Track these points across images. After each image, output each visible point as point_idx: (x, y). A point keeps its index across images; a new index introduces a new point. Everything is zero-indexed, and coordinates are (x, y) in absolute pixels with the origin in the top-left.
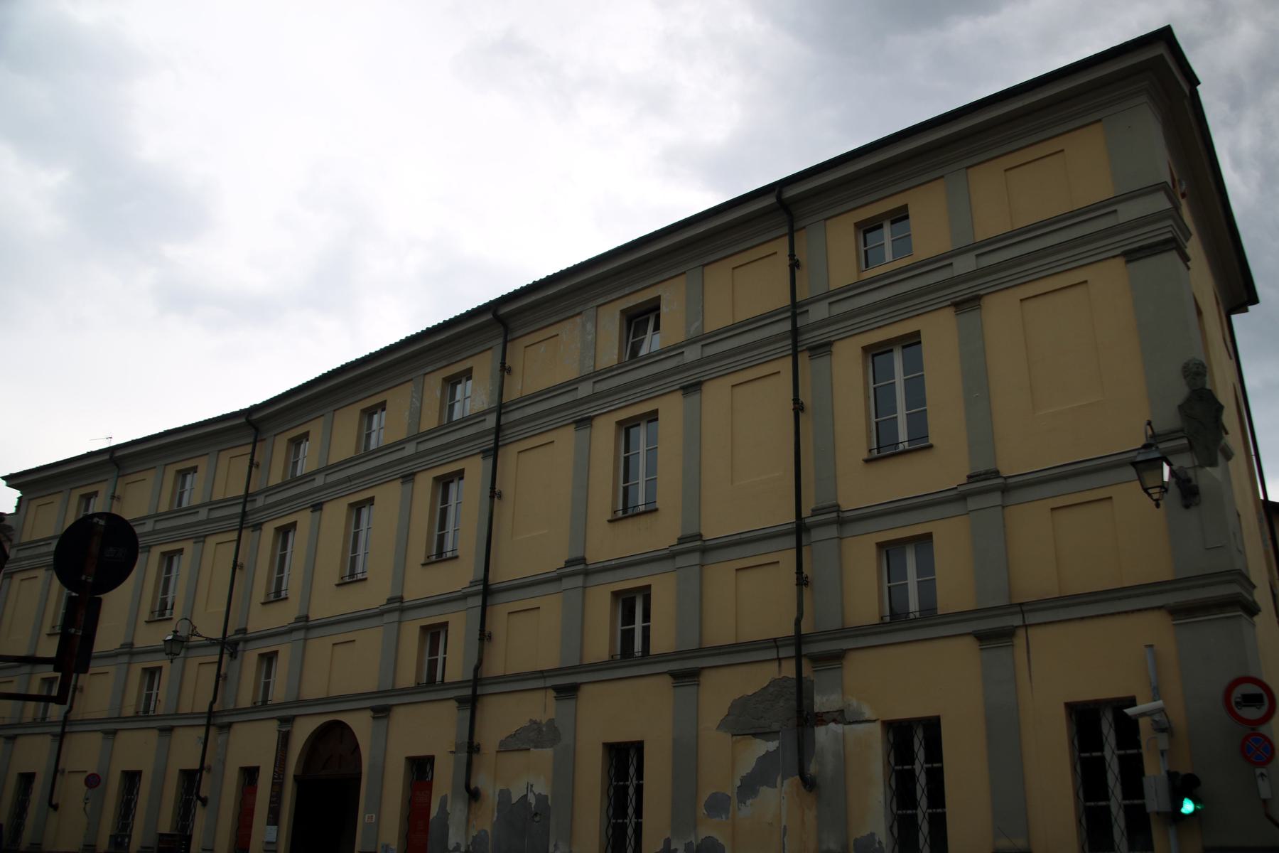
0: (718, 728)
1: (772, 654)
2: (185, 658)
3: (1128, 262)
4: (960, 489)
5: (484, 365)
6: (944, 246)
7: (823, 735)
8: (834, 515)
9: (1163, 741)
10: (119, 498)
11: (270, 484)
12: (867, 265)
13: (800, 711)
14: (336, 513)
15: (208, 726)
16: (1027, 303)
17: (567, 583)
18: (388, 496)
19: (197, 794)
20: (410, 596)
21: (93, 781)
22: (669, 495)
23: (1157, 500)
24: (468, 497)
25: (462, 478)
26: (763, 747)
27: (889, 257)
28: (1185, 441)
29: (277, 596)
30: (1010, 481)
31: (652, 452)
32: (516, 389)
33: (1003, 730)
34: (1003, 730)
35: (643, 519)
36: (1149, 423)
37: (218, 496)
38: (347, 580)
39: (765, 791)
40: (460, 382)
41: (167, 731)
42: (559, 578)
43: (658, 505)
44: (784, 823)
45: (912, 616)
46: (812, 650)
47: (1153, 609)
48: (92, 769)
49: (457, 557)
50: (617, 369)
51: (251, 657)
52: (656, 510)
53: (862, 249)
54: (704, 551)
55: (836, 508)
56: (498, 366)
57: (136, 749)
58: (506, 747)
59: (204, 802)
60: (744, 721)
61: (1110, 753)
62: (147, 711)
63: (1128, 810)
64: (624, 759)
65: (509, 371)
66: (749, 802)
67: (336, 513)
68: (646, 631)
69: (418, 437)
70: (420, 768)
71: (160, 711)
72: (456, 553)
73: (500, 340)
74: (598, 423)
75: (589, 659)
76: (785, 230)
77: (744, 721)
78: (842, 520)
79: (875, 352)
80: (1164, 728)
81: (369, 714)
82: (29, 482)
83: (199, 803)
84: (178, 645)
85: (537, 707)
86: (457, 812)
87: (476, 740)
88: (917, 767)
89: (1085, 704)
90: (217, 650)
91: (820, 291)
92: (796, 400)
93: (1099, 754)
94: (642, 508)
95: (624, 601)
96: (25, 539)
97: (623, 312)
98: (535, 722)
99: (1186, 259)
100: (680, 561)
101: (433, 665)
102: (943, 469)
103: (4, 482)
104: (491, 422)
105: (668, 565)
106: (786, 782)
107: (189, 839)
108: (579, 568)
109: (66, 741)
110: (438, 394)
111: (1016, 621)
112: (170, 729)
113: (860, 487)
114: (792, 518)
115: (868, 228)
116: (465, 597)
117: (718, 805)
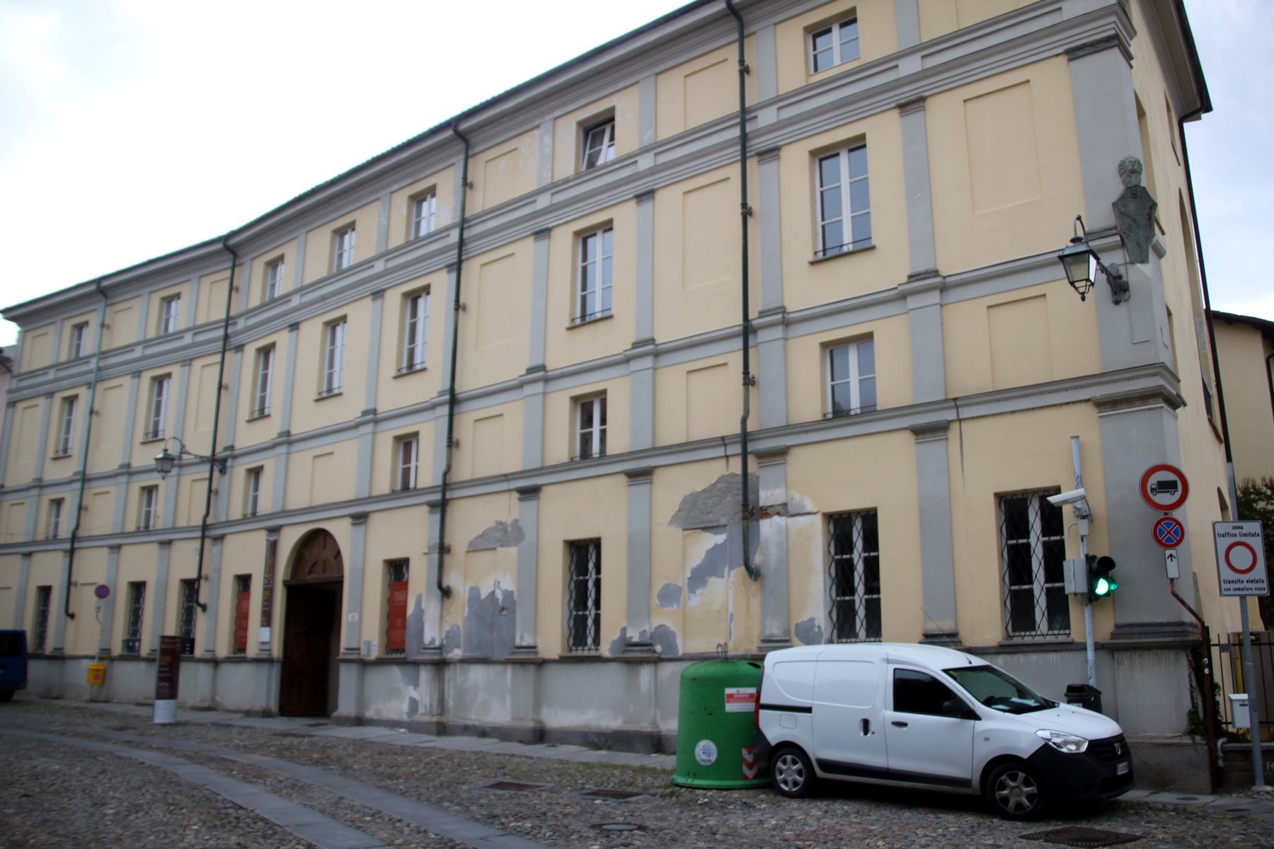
0: (671, 523)
1: (720, 452)
2: (179, 476)
3: (1070, 60)
4: (900, 288)
5: (447, 181)
6: (891, 48)
7: (768, 527)
8: (779, 316)
9: (1083, 527)
10: (108, 327)
11: (781, 92)
12: (816, 69)
13: (745, 505)
14: (312, 331)
15: (203, 538)
16: (970, 104)
17: (529, 390)
18: (360, 313)
20: (384, 407)
21: (102, 592)
22: (623, 305)
23: (1083, 294)
24: (435, 309)
25: (428, 293)
26: (712, 540)
27: (837, 61)
28: (1118, 238)
29: (261, 414)
30: (948, 280)
31: (607, 259)
32: (477, 204)
34: (936, 523)
35: (600, 325)
36: (1079, 218)
37: (201, 320)
38: (325, 395)
39: (713, 581)
40: (425, 199)
41: (167, 544)
42: (627, 360)
43: (874, 242)
44: (731, 610)
45: (853, 413)
46: (755, 448)
47: (1080, 401)
48: (102, 582)
49: (611, 317)
50: (575, 179)
51: (239, 471)
52: (873, 248)
53: (811, 53)
54: (657, 354)
55: (782, 310)
56: (460, 181)
57: (140, 562)
58: (474, 548)
59: (204, 607)
60: (694, 517)
61: (1036, 540)
62: (147, 527)
63: (1049, 592)
64: (583, 554)
65: (471, 186)
66: (698, 592)
67: (312, 331)
68: (603, 433)
69: (146, 343)
70: (397, 569)
71: (160, 526)
72: (424, 366)
73: (462, 157)
74: (556, 234)
75: (550, 461)
76: (736, 36)
77: (694, 517)
78: (787, 321)
79: (823, 156)
80: (1086, 516)
81: (348, 521)
82: (28, 315)
83: (199, 610)
84: (168, 462)
85: (505, 508)
86: (432, 608)
87: (447, 541)
88: (856, 556)
89: (1014, 493)
90: (207, 467)
91: (771, 95)
92: (744, 205)
93: (1024, 541)
94: (599, 316)
95: (583, 406)
96: (24, 369)
97: (580, 124)
98: (501, 523)
99: (1128, 57)
100: (635, 365)
101: (406, 472)
104: (454, 236)
105: (621, 370)
106: (732, 573)
107: (192, 642)
108: (540, 374)
109: (77, 555)
110: (404, 211)
111: (951, 415)
112: (169, 542)
113: (805, 288)
114: (739, 320)
115: (818, 31)
116: (434, 407)
117: (670, 595)
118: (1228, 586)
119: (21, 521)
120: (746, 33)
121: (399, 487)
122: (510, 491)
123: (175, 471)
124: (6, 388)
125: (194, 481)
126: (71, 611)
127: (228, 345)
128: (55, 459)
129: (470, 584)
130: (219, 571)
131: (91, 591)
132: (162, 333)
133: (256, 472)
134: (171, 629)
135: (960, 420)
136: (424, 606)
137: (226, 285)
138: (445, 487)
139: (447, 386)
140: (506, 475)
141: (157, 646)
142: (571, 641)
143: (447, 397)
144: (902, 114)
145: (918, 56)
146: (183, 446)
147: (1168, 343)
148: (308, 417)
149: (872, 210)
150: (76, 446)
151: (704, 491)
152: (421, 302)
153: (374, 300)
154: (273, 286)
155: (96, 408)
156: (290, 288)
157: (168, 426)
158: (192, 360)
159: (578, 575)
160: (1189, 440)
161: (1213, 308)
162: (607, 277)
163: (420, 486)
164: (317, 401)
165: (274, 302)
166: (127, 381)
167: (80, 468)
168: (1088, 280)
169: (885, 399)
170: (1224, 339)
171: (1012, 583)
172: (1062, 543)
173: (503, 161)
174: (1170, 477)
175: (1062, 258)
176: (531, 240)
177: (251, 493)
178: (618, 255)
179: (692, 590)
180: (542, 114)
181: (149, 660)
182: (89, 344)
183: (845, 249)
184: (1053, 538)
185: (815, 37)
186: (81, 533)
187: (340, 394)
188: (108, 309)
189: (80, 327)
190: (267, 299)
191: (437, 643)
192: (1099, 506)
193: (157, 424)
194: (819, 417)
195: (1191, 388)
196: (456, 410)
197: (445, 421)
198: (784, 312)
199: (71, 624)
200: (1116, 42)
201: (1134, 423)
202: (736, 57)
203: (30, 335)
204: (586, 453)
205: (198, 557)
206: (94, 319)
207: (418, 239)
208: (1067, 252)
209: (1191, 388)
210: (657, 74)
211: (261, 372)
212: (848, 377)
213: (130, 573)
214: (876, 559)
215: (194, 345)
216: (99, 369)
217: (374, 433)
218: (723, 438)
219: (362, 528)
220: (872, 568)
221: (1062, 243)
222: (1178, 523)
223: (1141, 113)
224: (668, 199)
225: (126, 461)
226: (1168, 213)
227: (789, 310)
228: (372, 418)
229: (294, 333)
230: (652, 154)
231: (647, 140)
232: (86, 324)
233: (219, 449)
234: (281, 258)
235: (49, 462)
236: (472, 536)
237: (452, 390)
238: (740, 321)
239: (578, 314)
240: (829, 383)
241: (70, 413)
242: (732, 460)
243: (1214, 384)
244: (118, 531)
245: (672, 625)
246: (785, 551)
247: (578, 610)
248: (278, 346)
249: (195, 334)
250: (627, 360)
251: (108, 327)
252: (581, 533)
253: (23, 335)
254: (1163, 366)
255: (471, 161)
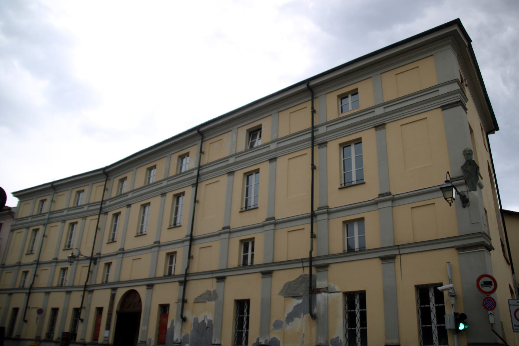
0: (279, 294)
1: (300, 265)
2: (77, 264)
3: (443, 110)
4: (375, 200)
5: (194, 151)
6: (371, 104)
7: (320, 297)
8: (326, 210)
9: (453, 300)
10: (54, 202)
12: (342, 112)
13: (310, 287)
14: (136, 208)
15: (84, 291)
16: (403, 126)
17: (222, 236)
18: (156, 202)
19: (80, 319)
20: (163, 241)
21: (40, 311)
22: (263, 203)
24: (186, 202)
25: (184, 195)
26: (296, 302)
27: (350, 109)
28: (464, 181)
31: (257, 184)
32: (206, 160)
33: (66, 309)
34: (66, 309)
35: (253, 211)
36: (448, 173)
38: (139, 234)
40: (184, 158)
42: (263, 226)
43: (365, 181)
44: (303, 332)
45: (356, 250)
46: (316, 263)
47: (450, 247)
48: (40, 307)
51: (102, 264)
52: (364, 183)
53: (340, 105)
54: (275, 224)
56: (199, 151)
57: (57, 300)
58: (197, 301)
59: (82, 320)
60: (289, 292)
61: (432, 305)
62: (62, 285)
64: (242, 306)
66: (290, 324)
67: (136, 208)
68: (252, 256)
69: (69, 209)
70: (164, 308)
71: (67, 285)
73: (200, 141)
76: (310, 98)
77: (289, 292)
79: (344, 146)
80: (453, 295)
81: (145, 287)
83: (80, 321)
84: (73, 259)
85: (210, 285)
86: (178, 326)
87: (186, 298)
88: (356, 310)
89: (423, 285)
90: (89, 261)
91: (324, 121)
92: (313, 164)
93: (428, 306)
94: (252, 207)
96: (19, 217)
98: (208, 291)
99: (466, 109)
100: (266, 228)
101: (170, 268)
102: (369, 192)
103: (12, 195)
104: (195, 173)
106: (305, 316)
107: (76, 335)
108: (227, 230)
110: (176, 162)
111: (397, 252)
112: (70, 292)
113: (337, 199)
114: (309, 211)
115: (343, 97)
116: (183, 241)
117: (278, 325)
118: (517, 328)
119: (9, 280)
120: (314, 97)
121: (167, 274)
122: (213, 278)
123: (75, 262)
124: (11, 224)
125: (83, 267)
126: (26, 319)
127: (102, 212)
128: (27, 254)
129: (194, 316)
130: (90, 305)
131: (35, 311)
132: (75, 205)
133: (109, 265)
134: (67, 329)
135: (400, 254)
136: (174, 325)
137: (103, 188)
138: (186, 275)
139: (189, 233)
140: (211, 271)
141: (60, 336)
142: (236, 343)
143: (189, 238)
144: (376, 130)
145: (382, 108)
146: (80, 252)
147: (486, 223)
148: (131, 243)
149: (364, 154)
150: (36, 249)
151: (293, 281)
152: (181, 198)
153: (162, 197)
154: (121, 189)
155: (46, 234)
156: (128, 190)
157: (74, 244)
158: (86, 217)
159: (240, 315)
160: (496, 264)
161: (503, 208)
162: (256, 191)
163: (176, 274)
164: (136, 236)
165: (121, 195)
166: (59, 224)
167: (37, 259)
168: (452, 198)
169: (370, 244)
170: (510, 224)
171: (423, 324)
172: (444, 307)
173: (216, 144)
174: (489, 280)
175: (441, 189)
176: (226, 175)
177: (106, 273)
178: (261, 183)
179: (287, 323)
180: (233, 126)
181: (56, 342)
182: (46, 208)
183: (353, 183)
184: (440, 305)
185: (342, 99)
186: (35, 286)
187: (146, 234)
188: (55, 194)
189: (43, 201)
190: (119, 194)
191: (179, 341)
192: (459, 291)
193: (70, 242)
194: (342, 252)
195: (496, 242)
196: (192, 244)
197: (188, 247)
198: (328, 208)
199: (25, 325)
200: (460, 103)
201: (473, 257)
202: (310, 106)
203: (23, 203)
204: (245, 264)
205: (81, 299)
206: (49, 198)
207: (181, 173)
208: (443, 186)
209: (496, 242)
210: (279, 112)
211: (114, 223)
212: (354, 235)
213: (53, 304)
214: (365, 312)
215: (88, 211)
216: (49, 218)
217: (158, 251)
218: (302, 259)
219: (151, 290)
220: (363, 315)
221: (441, 181)
222: (493, 299)
223: (471, 131)
224: (282, 162)
225: (56, 257)
226: (483, 171)
227: (330, 207)
228: (158, 245)
229: (129, 208)
230: (276, 143)
231: (274, 138)
232: (46, 200)
233: (94, 254)
234: (125, 178)
235: (24, 256)
236: (196, 296)
237: (191, 235)
238: (310, 211)
239: (244, 206)
240: (346, 238)
241: (35, 236)
242: (305, 269)
243: (505, 240)
244: (49, 286)
245: (279, 338)
246: (327, 308)
247: (239, 330)
248: (122, 213)
249: (89, 207)
250: (263, 226)
251: (54, 202)
252: (241, 297)
253: (20, 203)
254: (484, 233)
255: (204, 143)
